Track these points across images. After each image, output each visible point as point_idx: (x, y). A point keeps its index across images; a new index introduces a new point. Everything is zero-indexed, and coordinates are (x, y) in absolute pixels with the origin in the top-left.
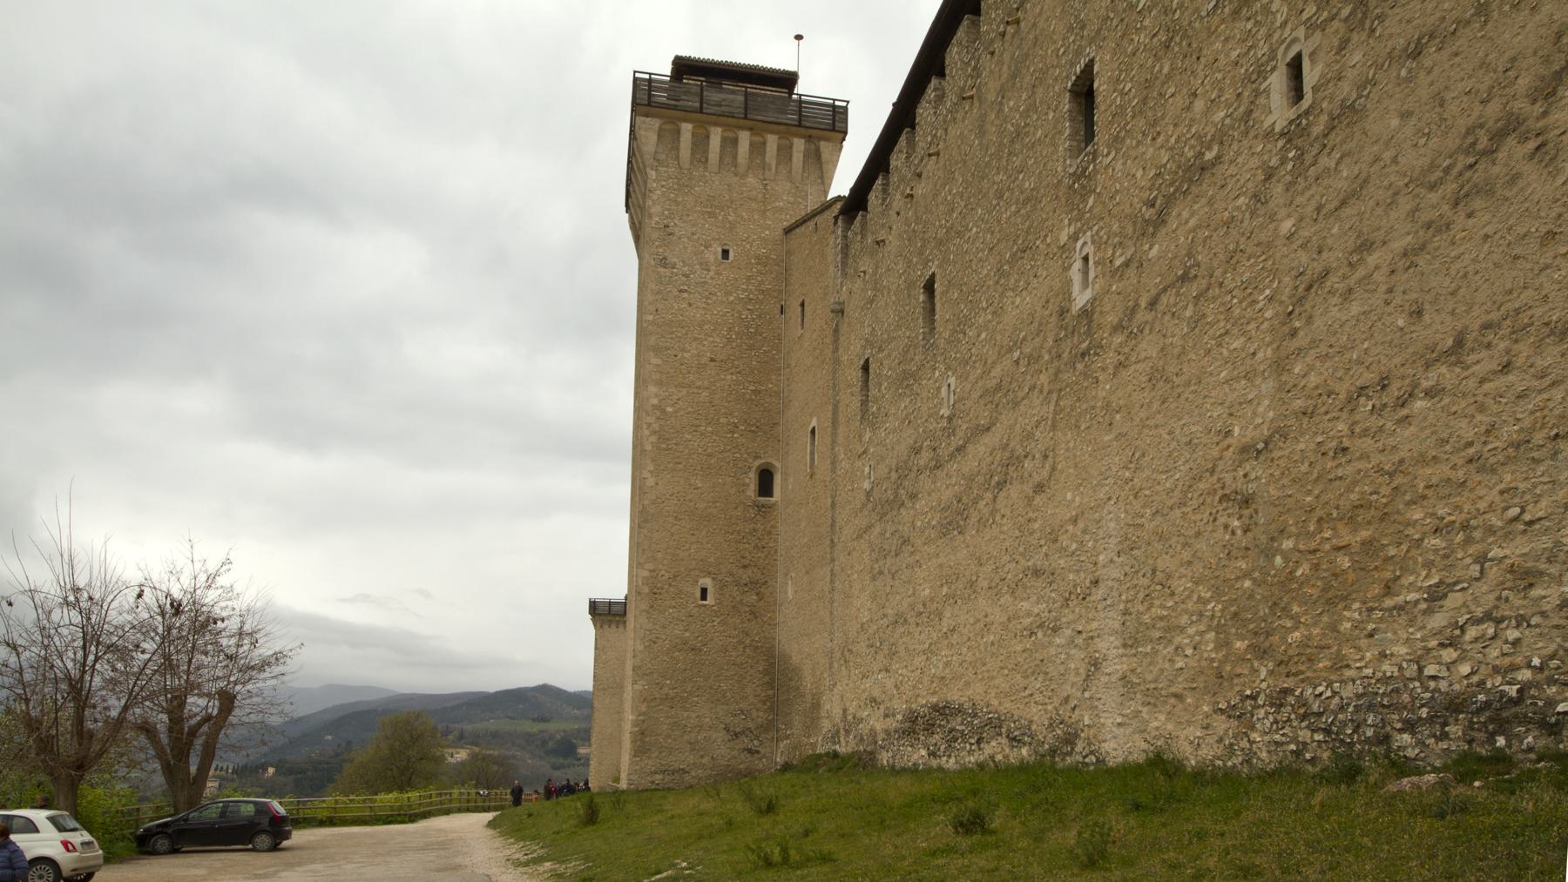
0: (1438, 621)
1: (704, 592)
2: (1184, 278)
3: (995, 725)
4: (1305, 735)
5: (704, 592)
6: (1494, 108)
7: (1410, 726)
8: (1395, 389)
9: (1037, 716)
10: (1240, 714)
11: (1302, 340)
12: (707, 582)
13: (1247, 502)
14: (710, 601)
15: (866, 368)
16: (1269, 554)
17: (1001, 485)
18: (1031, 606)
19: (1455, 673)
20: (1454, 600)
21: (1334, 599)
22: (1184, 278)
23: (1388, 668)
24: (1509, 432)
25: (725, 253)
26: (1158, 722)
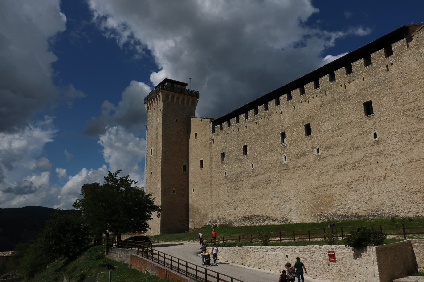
0: (338, 208)
1: (174, 191)
2: (304, 166)
3: (269, 218)
4: (324, 219)
5: (174, 191)
6: (340, 164)
7: (336, 218)
8: (332, 186)
9: (279, 217)
10: (316, 216)
11: (321, 178)
12: (174, 189)
13: (315, 194)
14: (175, 193)
15: (223, 154)
16: (318, 199)
17: (268, 183)
18: (276, 201)
19: (340, 213)
20: (339, 206)
21: (327, 205)
22: (304, 166)
23: (333, 212)
24: (343, 193)
25: (177, 120)
26: (303, 217)
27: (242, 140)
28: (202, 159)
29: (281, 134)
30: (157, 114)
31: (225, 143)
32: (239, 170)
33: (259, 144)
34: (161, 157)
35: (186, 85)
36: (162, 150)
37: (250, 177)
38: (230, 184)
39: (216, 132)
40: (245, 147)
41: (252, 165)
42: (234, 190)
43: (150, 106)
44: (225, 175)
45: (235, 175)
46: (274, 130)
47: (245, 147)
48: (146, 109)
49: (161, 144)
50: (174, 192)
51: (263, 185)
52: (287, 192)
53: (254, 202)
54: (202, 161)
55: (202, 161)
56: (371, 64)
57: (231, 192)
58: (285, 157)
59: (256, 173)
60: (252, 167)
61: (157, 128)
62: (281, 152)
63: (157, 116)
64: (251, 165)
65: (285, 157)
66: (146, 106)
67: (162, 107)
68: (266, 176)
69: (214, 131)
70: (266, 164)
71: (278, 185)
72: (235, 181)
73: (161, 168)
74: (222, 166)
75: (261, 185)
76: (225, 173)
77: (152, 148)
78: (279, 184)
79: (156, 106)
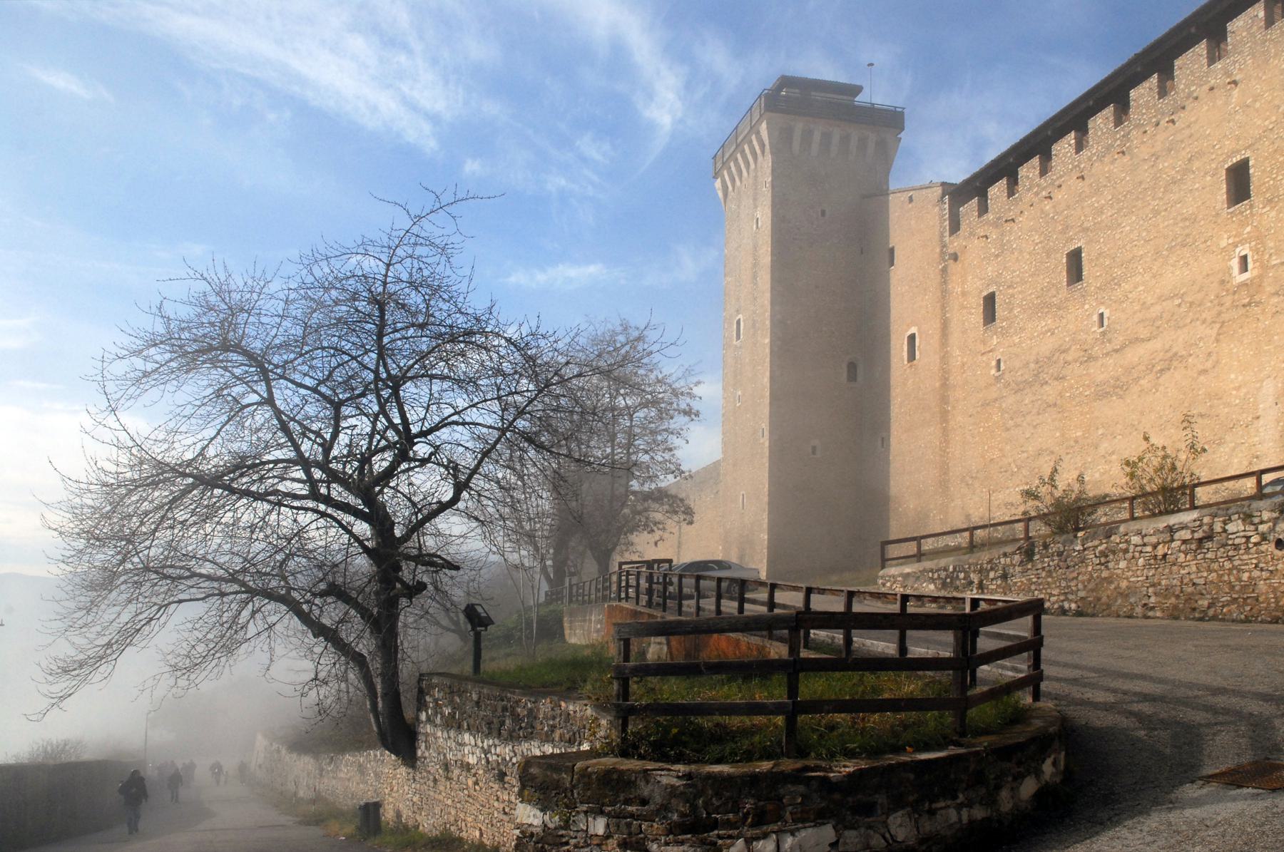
27: (1063, 232)
28: (913, 330)
29: (1228, 170)
30: (755, 199)
31: (997, 256)
32: (1048, 345)
33: (1131, 231)
34: (767, 341)
35: (857, 90)
36: (772, 316)
37: (1091, 358)
38: (1011, 400)
39: (963, 227)
40: (1075, 259)
41: (1102, 315)
42: (1029, 418)
43: (733, 181)
44: (993, 372)
45: (1032, 366)
46: (1196, 165)
47: (1075, 259)
48: (720, 194)
49: (768, 295)
50: (814, 453)
51: (1142, 382)
52: (1244, 390)
53: (1102, 450)
54: (912, 338)
55: (912, 338)
56: (1248, 197)
57: (1017, 426)
58: (1244, 259)
59: (1119, 340)
60: (1102, 325)
61: (755, 248)
62: (1223, 243)
63: (756, 207)
64: (1095, 318)
65: (1244, 259)
66: (718, 183)
67: (769, 171)
68: (1156, 345)
69: (955, 227)
70: (1162, 299)
71: (1205, 371)
72: (1030, 384)
73: (768, 374)
74: (984, 342)
75: (1137, 380)
76: (994, 363)
77: (740, 316)
78: (1209, 364)
79: (752, 174)
